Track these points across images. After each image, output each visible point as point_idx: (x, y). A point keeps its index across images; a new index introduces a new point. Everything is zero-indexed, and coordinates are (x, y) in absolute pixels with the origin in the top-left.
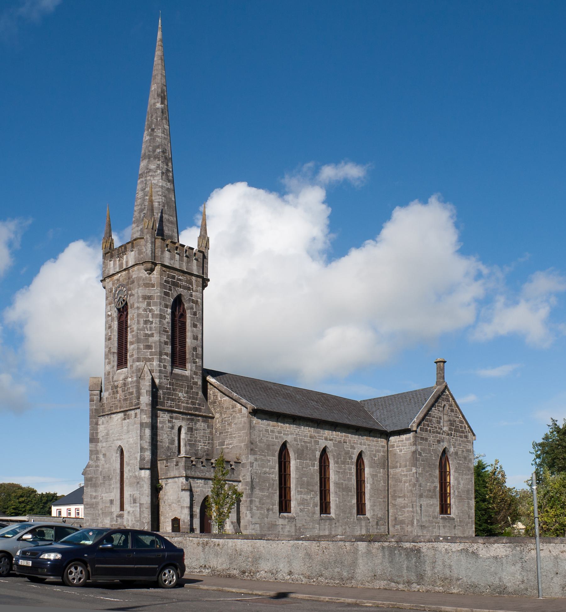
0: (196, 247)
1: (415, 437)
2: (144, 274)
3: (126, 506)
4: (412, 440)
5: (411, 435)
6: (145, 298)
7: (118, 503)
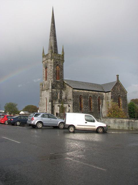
0: (61, 54)
1: (112, 93)
2: (50, 61)
3: (47, 110)
4: (111, 94)
5: (111, 92)
6: (50, 66)
7: (46, 110)
